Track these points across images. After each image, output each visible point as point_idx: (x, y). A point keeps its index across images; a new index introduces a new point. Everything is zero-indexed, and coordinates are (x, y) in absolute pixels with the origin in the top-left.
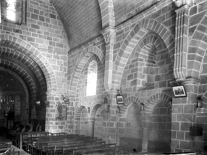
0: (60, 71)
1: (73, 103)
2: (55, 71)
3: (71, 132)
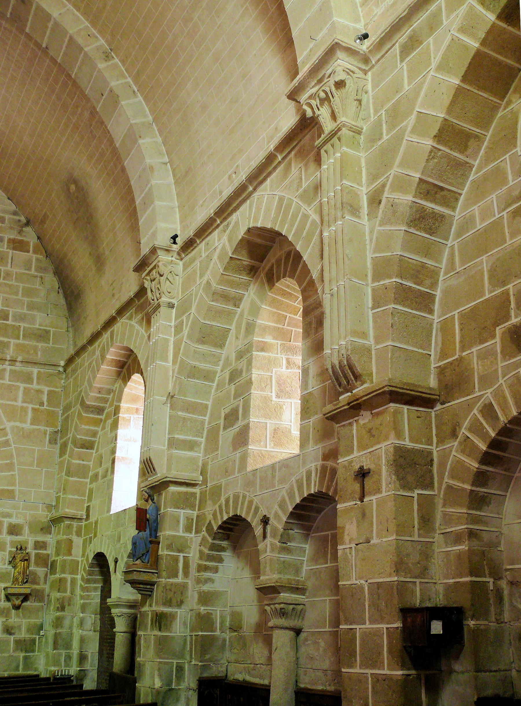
0: (32, 424)
1: (71, 541)
2: (12, 424)
3: (59, 665)
